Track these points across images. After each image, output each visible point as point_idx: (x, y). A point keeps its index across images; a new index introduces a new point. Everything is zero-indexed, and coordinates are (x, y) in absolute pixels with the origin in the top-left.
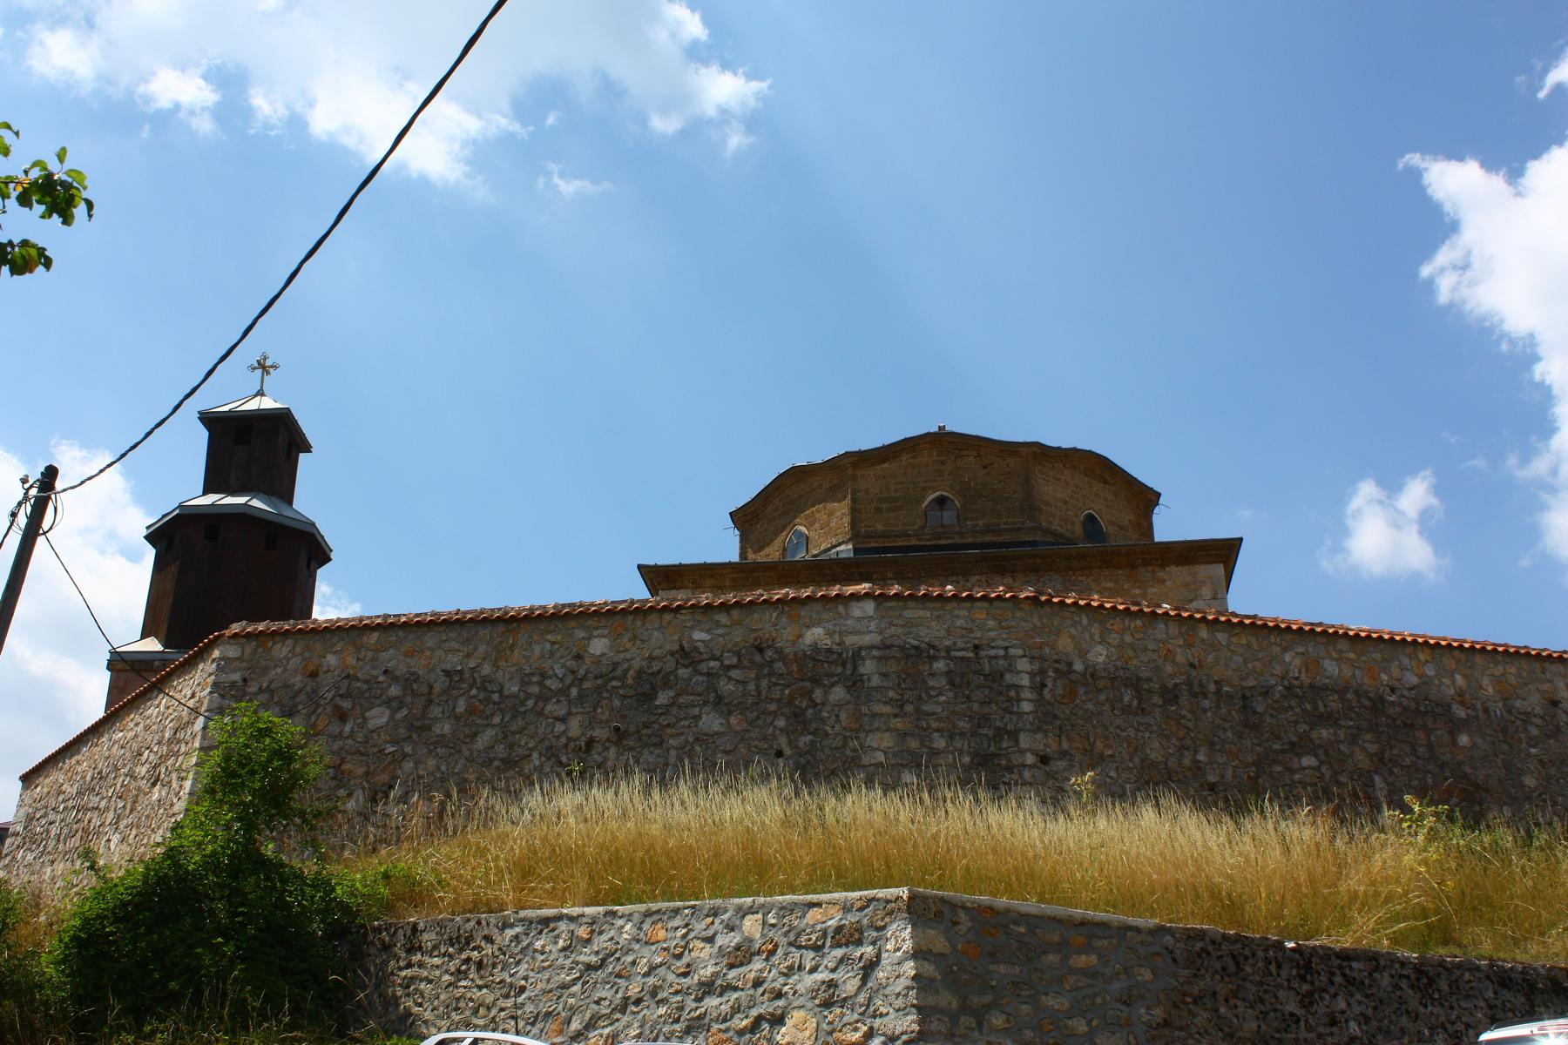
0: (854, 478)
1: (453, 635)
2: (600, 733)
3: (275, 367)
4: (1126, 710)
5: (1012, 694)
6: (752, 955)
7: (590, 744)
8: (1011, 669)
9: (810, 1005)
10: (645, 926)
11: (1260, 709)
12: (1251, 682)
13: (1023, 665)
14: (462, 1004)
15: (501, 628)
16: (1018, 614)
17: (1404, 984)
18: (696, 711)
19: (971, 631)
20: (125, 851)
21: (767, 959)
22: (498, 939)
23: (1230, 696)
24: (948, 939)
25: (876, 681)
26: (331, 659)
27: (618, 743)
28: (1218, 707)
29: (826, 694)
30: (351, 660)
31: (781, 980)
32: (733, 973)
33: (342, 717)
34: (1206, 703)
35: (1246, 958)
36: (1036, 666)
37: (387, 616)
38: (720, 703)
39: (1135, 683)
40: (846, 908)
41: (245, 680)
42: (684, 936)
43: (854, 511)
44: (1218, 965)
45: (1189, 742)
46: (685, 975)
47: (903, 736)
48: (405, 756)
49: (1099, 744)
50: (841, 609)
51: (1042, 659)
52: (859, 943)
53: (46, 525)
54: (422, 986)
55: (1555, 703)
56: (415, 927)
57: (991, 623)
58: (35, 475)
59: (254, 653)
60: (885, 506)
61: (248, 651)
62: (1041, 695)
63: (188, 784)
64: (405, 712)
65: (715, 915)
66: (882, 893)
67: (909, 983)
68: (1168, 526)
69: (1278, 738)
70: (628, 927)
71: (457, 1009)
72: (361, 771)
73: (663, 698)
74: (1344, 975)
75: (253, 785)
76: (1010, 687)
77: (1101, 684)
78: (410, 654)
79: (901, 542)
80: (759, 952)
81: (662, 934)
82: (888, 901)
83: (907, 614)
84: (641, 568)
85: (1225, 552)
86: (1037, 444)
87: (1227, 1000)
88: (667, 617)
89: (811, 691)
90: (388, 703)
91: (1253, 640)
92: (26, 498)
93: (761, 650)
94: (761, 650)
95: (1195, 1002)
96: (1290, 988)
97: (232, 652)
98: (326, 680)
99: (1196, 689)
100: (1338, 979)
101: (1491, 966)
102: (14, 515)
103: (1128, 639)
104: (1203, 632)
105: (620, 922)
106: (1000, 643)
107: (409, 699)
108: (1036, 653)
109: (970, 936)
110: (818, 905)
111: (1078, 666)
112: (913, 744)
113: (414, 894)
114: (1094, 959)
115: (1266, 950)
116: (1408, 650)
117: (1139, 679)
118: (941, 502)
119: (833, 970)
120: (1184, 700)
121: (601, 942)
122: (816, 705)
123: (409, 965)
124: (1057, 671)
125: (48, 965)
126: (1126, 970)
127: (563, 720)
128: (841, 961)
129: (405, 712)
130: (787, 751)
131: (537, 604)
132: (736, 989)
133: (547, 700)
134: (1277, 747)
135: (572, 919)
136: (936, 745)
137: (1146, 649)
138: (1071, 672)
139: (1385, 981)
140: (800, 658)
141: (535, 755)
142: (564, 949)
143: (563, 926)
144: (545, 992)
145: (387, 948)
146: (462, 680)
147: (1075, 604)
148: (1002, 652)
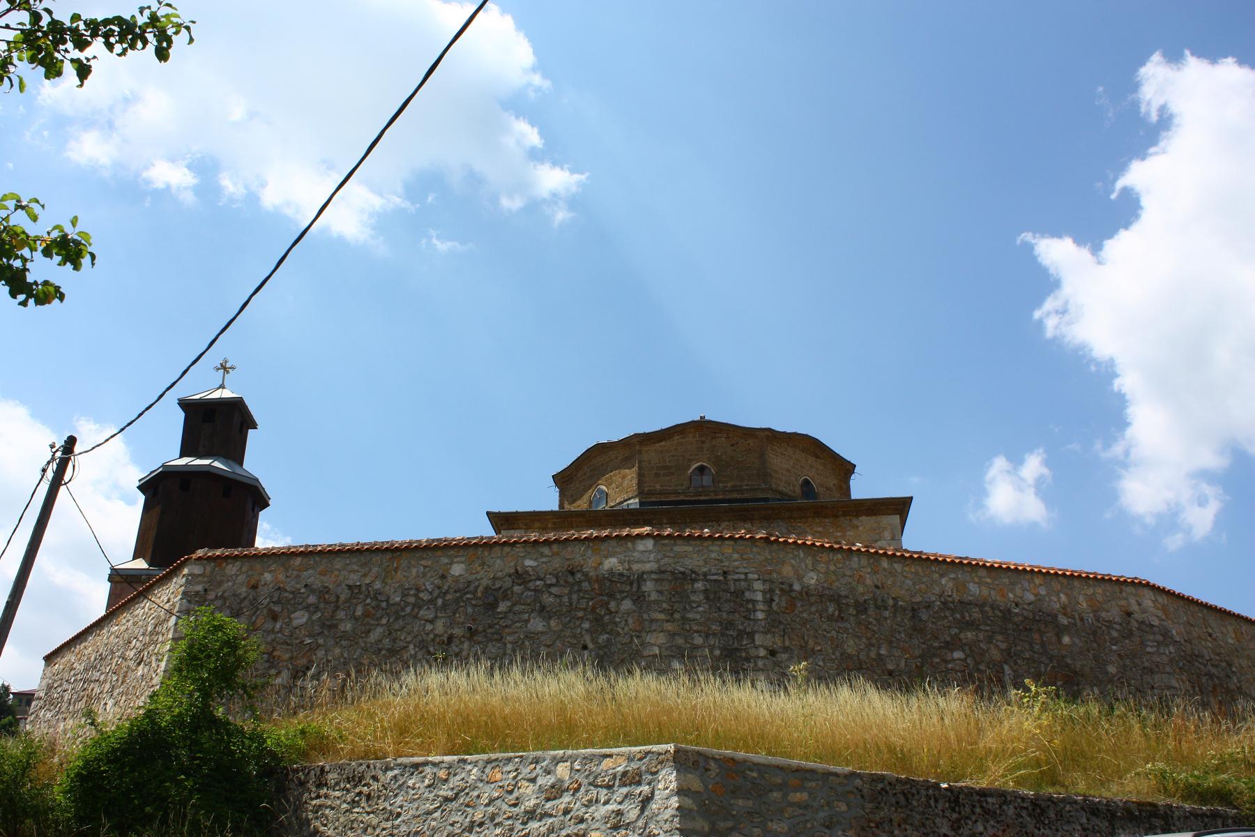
0: (640, 452)
1: (355, 560)
2: (457, 631)
3: (232, 368)
4: (830, 618)
5: (750, 606)
6: (563, 791)
7: (450, 638)
8: (750, 588)
9: (603, 827)
10: (487, 770)
11: (924, 617)
12: (918, 599)
13: (758, 586)
14: (355, 825)
15: (389, 555)
16: (755, 550)
17: (1024, 813)
18: (526, 616)
19: (721, 561)
20: (116, 712)
21: (573, 795)
22: (382, 778)
23: (904, 609)
24: (702, 781)
25: (654, 596)
26: (268, 577)
27: (470, 639)
28: (895, 616)
29: (618, 606)
30: (281, 577)
31: (583, 810)
32: (549, 805)
33: (274, 617)
34: (887, 614)
35: (913, 795)
36: (767, 587)
37: (307, 546)
38: (542, 610)
39: (836, 599)
40: (630, 759)
41: (206, 590)
42: (515, 778)
43: (641, 476)
44: (893, 800)
45: (874, 641)
46: (515, 805)
47: (673, 635)
48: (319, 646)
49: (811, 643)
50: (630, 545)
51: (771, 581)
52: (639, 783)
53: (66, 478)
54: (327, 811)
55: (1129, 614)
56: (322, 768)
57: (736, 556)
58: (60, 443)
59: (212, 572)
60: (662, 472)
61: (208, 569)
62: (770, 607)
63: (163, 664)
64: (319, 614)
65: (537, 763)
66: (655, 748)
67: (674, 812)
68: (860, 489)
69: (937, 638)
70: (475, 771)
71: (352, 828)
72: (287, 656)
73: (502, 607)
74: (982, 807)
75: (210, 666)
76: (748, 601)
77: (813, 599)
78: (323, 573)
79: (672, 498)
80: (567, 790)
81: (499, 776)
82: (660, 754)
83: (677, 549)
84: (488, 513)
85: (900, 507)
86: (769, 430)
87: (899, 825)
88: (507, 549)
89: (608, 603)
90: (307, 608)
91: (920, 570)
92: (53, 459)
93: (573, 574)
94: (573, 574)
95: (877, 827)
96: (944, 817)
97: (197, 570)
98: (263, 591)
99: (879, 603)
100: (978, 810)
101: (1085, 800)
102: (44, 470)
103: (832, 568)
104: (885, 563)
105: (469, 767)
106: (741, 570)
107: (322, 605)
108: (767, 577)
109: (718, 779)
110: (610, 756)
111: (797, 587)
112: (680, 641)
113: (322, 745)
114: (805, 796)
115: (927, 789)
116: (1028, 577)
117: (840, 596)
118: (701, 469)
119: (620, 803)
120: (871, 611)
121: (455, 781)
122: (611, 613)
123: (318, 797)
124: (782, 590)
125: (58, 794)
126: (828, 804)
127: (431, 622)
128: (626, 796)
129: (319, 614)
130: (590, 646)
131: (414, 538)
132: (551, 816)
133: (420, 608)
134: (936, 644)
135: (435, 764)
136: (696, 642)
137: (844, 575)
138: (791, 590)
139: (1011, 811)
140: (600, 580)
141: (411, 646)
142: (429, 786)
143: (428, 769)
144: (415, 817)
145: (302, 784)
146: (360, 592)
147: (795, 543)
148: (743, 577)
